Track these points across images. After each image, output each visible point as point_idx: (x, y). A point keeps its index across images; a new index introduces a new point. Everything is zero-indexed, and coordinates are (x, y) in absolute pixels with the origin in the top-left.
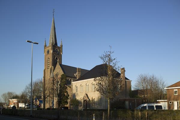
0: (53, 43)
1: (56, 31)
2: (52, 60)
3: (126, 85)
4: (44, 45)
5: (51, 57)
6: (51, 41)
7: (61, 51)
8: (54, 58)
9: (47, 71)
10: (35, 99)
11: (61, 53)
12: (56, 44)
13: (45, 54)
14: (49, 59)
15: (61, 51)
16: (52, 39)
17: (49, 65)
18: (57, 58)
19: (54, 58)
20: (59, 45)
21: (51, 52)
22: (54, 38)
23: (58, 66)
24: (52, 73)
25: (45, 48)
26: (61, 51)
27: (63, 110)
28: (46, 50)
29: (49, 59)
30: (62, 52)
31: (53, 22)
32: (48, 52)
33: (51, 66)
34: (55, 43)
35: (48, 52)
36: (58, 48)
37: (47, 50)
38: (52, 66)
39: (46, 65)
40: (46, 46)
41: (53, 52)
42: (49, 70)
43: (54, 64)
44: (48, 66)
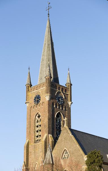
0: (51, 77)
1: (53, 39)
2: (49, 119)
3: (50, 70)
4: (27, 82)
5: (47, 110)
6: (48, 73)
7: (69, 96)
8: (53, 115)
9: (35, 147)
10: (41, 163)
11: (70, 103)
12: (56, 80)
13: (27, 105)
14: (39, 117)
15: (69, 96)
16: (48, 68)
17: (40, 133)
18: (59, 115)
19: (53, 115)
20: (63, 82)
21: (46, 98)
22: (51, 66)
23: (65, 134)
24: (48, 153)
25: (28, 91)
26: (69, 98)
27: (84, 159)
28: (32, 95)
29: (39, 117)
30: (71, 101)
31: (47, 29)
32: (37, 99)
33: (46, 135)
34: (54, 79)
35: (37, 99)
36: (62, 90)
37: (34, 96)
38: (49, 133)
39: (32, 132)
40: (31, 85)
41: (52, 98)
42: (41, 144)
43: (53, 129)
44: (37, 134)
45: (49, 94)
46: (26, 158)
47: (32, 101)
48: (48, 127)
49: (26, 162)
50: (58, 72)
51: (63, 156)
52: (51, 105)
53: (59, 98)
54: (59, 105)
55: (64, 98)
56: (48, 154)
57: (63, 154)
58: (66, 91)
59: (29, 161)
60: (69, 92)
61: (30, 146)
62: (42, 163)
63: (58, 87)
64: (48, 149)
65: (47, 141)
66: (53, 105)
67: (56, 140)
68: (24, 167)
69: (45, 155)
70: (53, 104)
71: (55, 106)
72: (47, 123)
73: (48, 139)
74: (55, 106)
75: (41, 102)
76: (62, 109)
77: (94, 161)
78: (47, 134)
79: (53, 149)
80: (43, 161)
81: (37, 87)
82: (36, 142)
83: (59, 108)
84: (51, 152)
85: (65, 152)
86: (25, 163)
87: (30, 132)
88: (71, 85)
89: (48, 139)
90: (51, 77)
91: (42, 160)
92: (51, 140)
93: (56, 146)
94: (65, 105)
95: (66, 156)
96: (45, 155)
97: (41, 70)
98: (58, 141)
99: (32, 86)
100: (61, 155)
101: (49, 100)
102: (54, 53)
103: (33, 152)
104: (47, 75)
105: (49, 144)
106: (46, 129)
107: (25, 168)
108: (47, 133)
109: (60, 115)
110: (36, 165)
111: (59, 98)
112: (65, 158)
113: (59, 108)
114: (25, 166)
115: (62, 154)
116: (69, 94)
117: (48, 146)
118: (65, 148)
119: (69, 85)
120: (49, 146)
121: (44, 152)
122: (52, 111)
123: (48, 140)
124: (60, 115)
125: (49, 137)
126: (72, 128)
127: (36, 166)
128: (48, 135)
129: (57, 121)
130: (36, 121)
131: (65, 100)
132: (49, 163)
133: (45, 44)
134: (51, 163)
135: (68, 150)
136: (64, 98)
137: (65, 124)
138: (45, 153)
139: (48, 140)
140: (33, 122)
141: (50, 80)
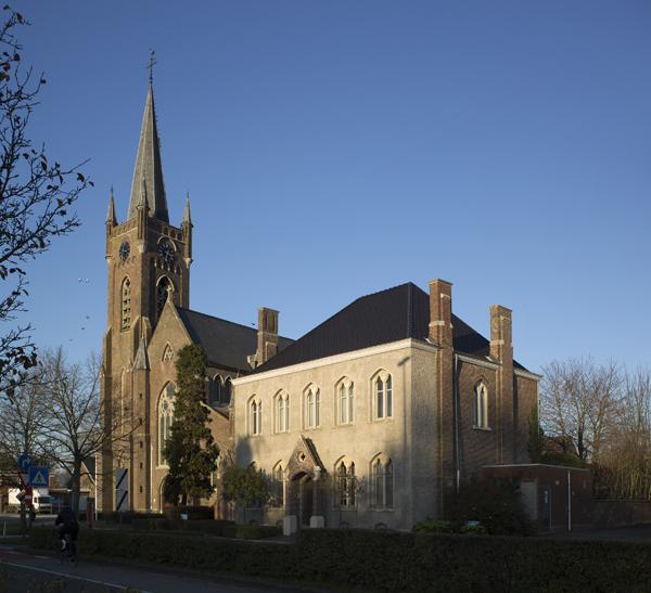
2: (143, 289)
4: (108, 216)
5: (139, 272)
6: (140, 199)
7: (187, 247)
11: (187, 260)
12: (162, 213)
13: (108, 260)
14: (128, 284)
15: (187, 247)
19: (152, 281)
20: (176, 219)
21: (139, 248)
24: (141, 350)
25: (110, 233)
26: (186, 251)
28: (117, 242)
29: (128, 284)
30: (190, 256)
31: (147, 109)
33: (137, 318)
35: (125, 250)
36: (173, 235)
39: (117, 313)
40: (115, 224)
41: (149, 248)
42: (130, 334)
45: (143, 241)
47: (116, 253)
49: (105, 365)
50: (463, 320)
52: (148, 263)
53: (166, 249)
54: (165, 264)
58: (180, 238)
60: (187, 239)
61: (113, 338)
64: (141, 342)
66: (152, 261)
67: (154, 325)
69: (135, 355)
75: (130, 256)
76: (172, 270)
77: (189, 363)
79: (148, 344)
81: (128, 226)
82: (123, 329)
83: (165, 268)
84: (146, 349)
88: (191, 226)
94: (179, 262)
96: (135, 355)
97: (134, 194)
98: (157, 329)
99: (117, 224)
106: (138, 307)
111: (166, 249)
113: (165, 268)
116: (186, 242)
122: (149, 272)
126: (196, 304)
131: (177, 254)
132: (141, 369)
137: (168, 301)
140: (118, 293)
141: (146, 214)
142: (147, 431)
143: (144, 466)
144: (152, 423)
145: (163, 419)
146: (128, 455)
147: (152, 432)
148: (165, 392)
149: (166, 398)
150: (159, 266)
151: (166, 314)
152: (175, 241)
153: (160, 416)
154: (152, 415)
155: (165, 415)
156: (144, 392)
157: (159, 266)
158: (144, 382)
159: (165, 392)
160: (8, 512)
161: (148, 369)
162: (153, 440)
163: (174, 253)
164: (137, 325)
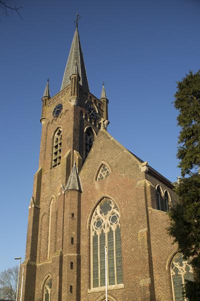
2: (75, 130)
5: (72, 119)
18: (89, 131)
24: (73, 174)
41: (80, 103)
45: (76, 96)
46: (37, 192)
48: (72, 139)
51: (99, 177)
54: (90, 118)
55: (97, 112)
56: (71, 177)
57: (98, 172)
59: (41, 196)
60: (105, 108)
62: (61, 191)
63: (89, 95)
65: (70, 159)
66: (81, 112)
68: (32, 206)
70: (81, 112)
71: (84, 117)
72: (72, 134)
73: (73, 156)
74: (84, 117)
78: (72, 150)
80: (64, 188)
83: (91, 122)
85: (102, 168)
86: (33, 199)
87: (45, 156)
89: (73, 156)
90: (79, 78)
91: (62, 186)
92: (77, 158)
93: (86, 163)
95: (103, 175)
100: (96, 174)
101: (75, 104)
102: (86, 77)
103: (48, 181)
104: (70, 188)
105: (74, 163)
107: (33, 206)
108: (72, 148)
109: (91, 134)
110: (51, 201)
112: (102, 178)
113: (91, 122)
114: (34, 203)
115: (96, 173)
117: (73, 166)
118: (103, 162)
119: (105, 100)
120: (74, 165)
121: (65, 174)
123: (73, 159)
124: (91, 134)
125: (75, 153)
127: (52, 202)
128: (73, 151)
129: (87, 139)
130: (55, 140)
131: (98, 116)
133: (72, 53)
134: (78, 189)
135: (108, 163)
136: (97, 112)
138: (66, 176)
139: (73, 159)
142: (78, 251)
143: (74, 290)
144: (83, 243)
145: (95, 237)
146: (107, 199)
147: (83, 251)
148: (98, 209)
149: (99, 215)
150: (86, 118)
151: (96, 152)
152: (97, 107)
153: (92, 234)
154: (84, 233)
155: (98, 233)
156: (75, 211)
157: (86, 118)
158: (76, 203)
159: (98, 209)
160: (86, 136)
161: (80, 191)
162: (84, 261)
163: (96, 114)
164: (69, 156)
